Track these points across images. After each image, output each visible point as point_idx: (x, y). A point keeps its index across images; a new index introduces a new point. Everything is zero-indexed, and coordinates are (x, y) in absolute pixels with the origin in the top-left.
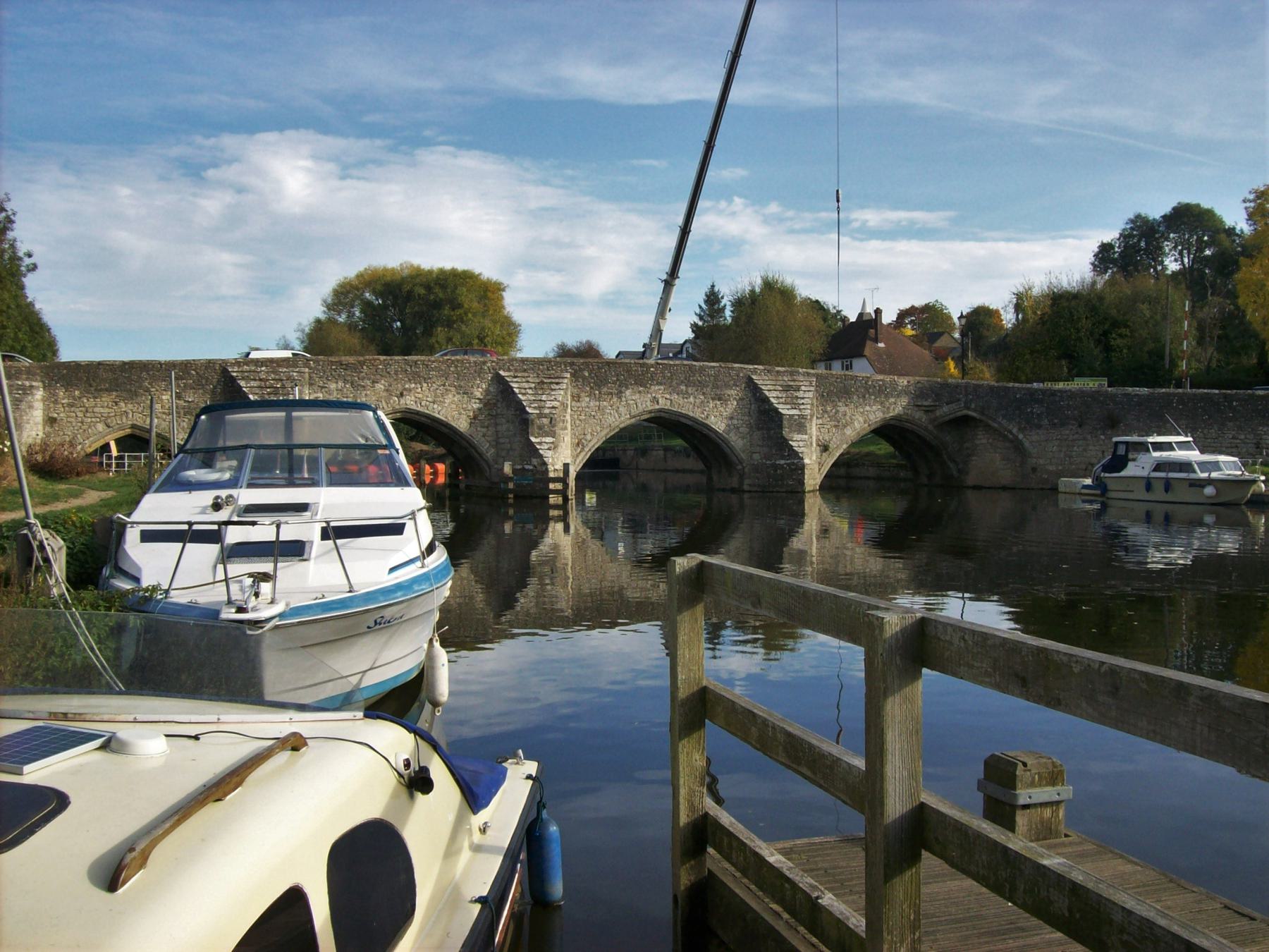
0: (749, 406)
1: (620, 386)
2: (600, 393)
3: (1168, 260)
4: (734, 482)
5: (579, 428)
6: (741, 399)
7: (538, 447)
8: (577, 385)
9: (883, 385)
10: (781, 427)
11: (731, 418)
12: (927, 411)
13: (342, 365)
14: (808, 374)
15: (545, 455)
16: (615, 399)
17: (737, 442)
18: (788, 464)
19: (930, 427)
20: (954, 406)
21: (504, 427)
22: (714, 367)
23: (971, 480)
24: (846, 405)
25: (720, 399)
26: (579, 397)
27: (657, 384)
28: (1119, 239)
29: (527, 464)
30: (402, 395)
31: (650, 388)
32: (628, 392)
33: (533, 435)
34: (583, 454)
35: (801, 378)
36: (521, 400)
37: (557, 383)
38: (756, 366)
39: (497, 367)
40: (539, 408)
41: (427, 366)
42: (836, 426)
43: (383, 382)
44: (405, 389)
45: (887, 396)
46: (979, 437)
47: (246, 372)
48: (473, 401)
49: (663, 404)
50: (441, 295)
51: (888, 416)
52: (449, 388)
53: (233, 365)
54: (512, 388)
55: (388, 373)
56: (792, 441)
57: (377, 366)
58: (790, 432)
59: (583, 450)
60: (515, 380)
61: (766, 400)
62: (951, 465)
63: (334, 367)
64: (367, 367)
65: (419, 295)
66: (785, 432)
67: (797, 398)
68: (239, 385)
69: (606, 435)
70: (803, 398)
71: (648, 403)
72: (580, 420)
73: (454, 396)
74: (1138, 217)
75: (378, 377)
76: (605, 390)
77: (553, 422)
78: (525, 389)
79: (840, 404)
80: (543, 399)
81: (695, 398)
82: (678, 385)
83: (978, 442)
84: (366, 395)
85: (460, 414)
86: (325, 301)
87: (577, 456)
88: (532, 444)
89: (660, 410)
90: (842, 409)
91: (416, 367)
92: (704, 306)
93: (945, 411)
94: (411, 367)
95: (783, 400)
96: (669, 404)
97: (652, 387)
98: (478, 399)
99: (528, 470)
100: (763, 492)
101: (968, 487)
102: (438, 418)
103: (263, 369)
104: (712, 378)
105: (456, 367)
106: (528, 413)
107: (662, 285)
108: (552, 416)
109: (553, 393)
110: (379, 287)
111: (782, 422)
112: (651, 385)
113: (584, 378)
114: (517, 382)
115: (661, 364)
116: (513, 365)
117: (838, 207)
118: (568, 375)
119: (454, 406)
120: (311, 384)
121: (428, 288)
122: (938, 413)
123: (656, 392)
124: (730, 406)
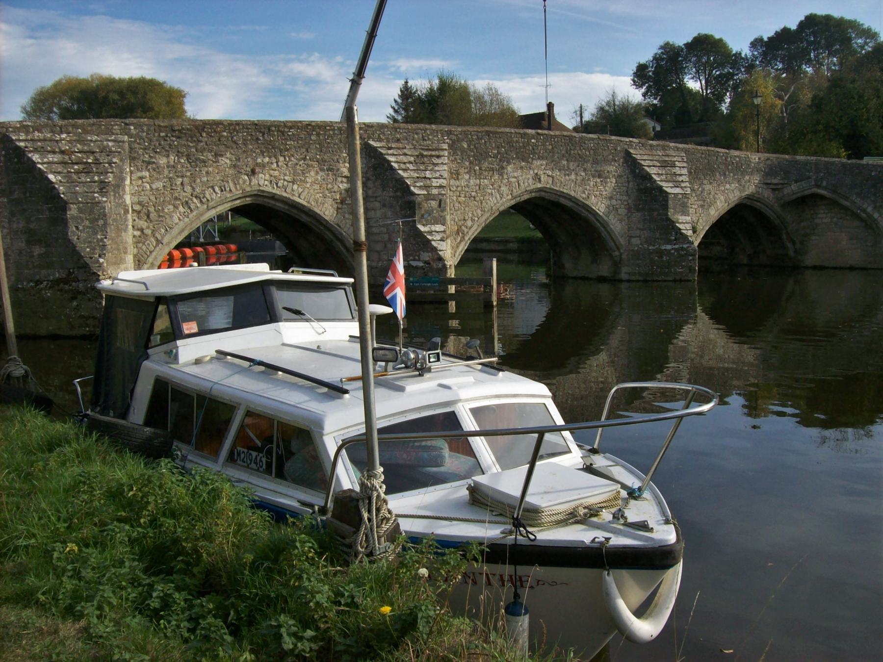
0: (627, 185)
1: (500, 160)
2: (480, 169)
3: (687, 77)
4: (605, 270)
5: (459, 212)
6: (620, 176)
7: (429, 237)
8: (455, 159)
9: (740, 161)
10: (666, 207)
11: (611, 198)
12: (773, 190)
13: (174, 131)
14: (678, 149)
15: (439, 248)
16: (496, 177)
17: (616, 226)
18: (676, 250)
19: (776, 206)
20: (804, 184)
21: (379, 214)
22: (593, 139)
23: (811, 259)
24: (711, 183)
25: (599, 176)
26: (458, 174)
27: (539, 158)
28: (652, 61)
29: (414, 260)
30: (253, 172)
31: (532, 164)
32: (510, 168)
33: (420, 222)
34: (463, 243)
35: (671, 152)
36: (403, 177)
37: (438, 157)
38: (631, 139)
39: (366, 136)
40: (426, 187)
41: (283, 133)
42: (702, 206)
43: (228, 155)
44: (257, 164)
45: (743, 173)
46: (820, 216)
47: (40, 140)
48: (339, 179)
49: (545, 182)
50: (133, 100)
51: (744, 194)
52: (311, 163)
53: (17, 130)
54: (389, 162)
55: (235, 142)
56: (679, 223)
57: (220, 132)
58: (674, 214)
59: (463, 239)
60: (390, 152)
61: (648, 177)
62: (789, 245)
63: (163, 134)
64: (208, 134)
65: (114, 100)
66: (671, 212)
67: (675, 174)
68: (30, 160)
69: (486, 220)
70: (681, 175)
71: (531, 181)
72: (459, 202)
73: (317, 173)
74: (667, 44)
75: (222, 148)
76: (486, 164)
77: (442, 205)
78: (405, 163)
79: (705, 182)
80: (428, 176)
81: (577, 174)
82: (560, 159)
83: (818, 221)
84: (207, 173)
85: (325, 197)
86: (24, 108)
87: (458, 247)
88: (420, 233)
89: (540, 190)
90: (708, 187)
91: (269, 134)
92: (399, 101)
93: (794, 189)
94: (263, 134)
95: (664, 177)
96: (551, 182)
97: (535, 162)
98: (345, 177)
99: (417, 268)
100: (645, 281)
101: (807, 268)
102: (299, 203)
103: (64, 136)
104: (592, 152)
105: (318, 135)
106: (413, 194)
107: (349, 84)
108: (440, 197)
109: (436, 168)
110: (75, 94)
111: (667, 201)
112: (533, 159)
113: (463, 151)
114: (393, 155)
115: (542, 135)
116: (383, 134)
117: (545, 6)
118: (445, 146)
119: (317, 187)
120: (132, 159)
121: (121, 94)
122: (786, 191)
123: (539, 167)
124: (609, 185)
